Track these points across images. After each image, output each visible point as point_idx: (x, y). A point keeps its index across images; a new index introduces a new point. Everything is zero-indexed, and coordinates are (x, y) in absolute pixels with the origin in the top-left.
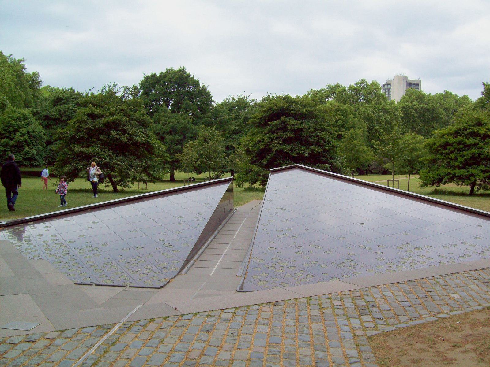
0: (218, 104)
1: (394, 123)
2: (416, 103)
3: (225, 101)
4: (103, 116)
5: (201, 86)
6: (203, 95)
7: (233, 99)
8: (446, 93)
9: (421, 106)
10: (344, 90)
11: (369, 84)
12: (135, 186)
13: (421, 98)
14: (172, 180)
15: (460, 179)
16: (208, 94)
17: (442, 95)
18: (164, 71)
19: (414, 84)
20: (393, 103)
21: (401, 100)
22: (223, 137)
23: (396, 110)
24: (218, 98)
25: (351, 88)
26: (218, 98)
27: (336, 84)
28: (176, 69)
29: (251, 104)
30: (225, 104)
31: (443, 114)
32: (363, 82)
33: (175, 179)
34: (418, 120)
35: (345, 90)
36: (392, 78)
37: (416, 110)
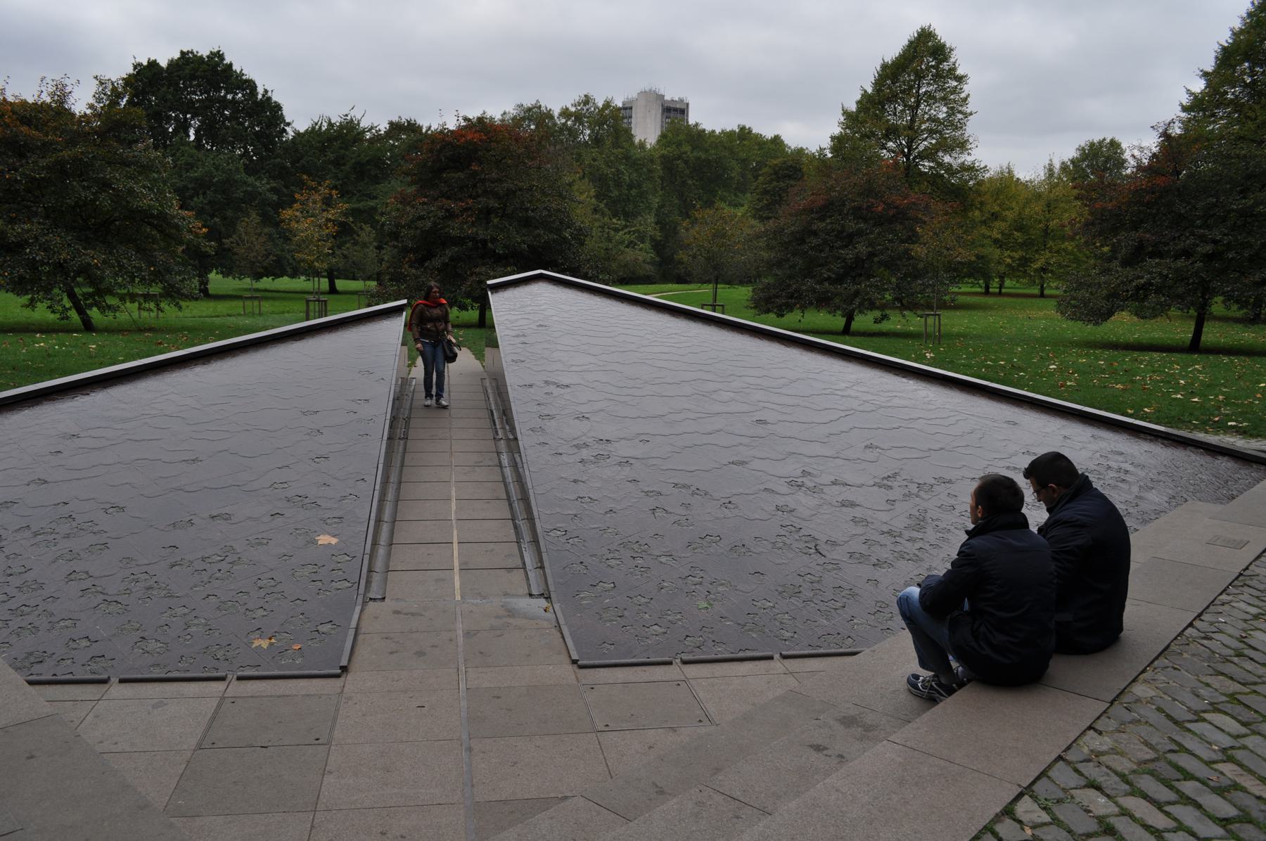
0: (298, 134)
1: (647, 186)
2: (686, 148)
3: (313, 128)
4: (46, 148)
5: (260, 90)
6: (269, 112)
7: (330, 124)
8: (743, 129)
9: (695, 154)
10: (549, 115)
11: (600, 105)
12: (130, 312)
13: (698, 137)
14: (206, 294)
15: (823, 302)
16: (278, 107)
17: (733, 132)
18: (177, 55)
19: (676, 110)
20: (642, 145)
21: (659, 141)
22: (915, 234)
23: (652, 161)
24: (299, 117)
25: (565, 113)
26: (299, 117)
27: (534, 102)
28: (204, 52)
29: (368, 136)
30: (313, 132)
31: (735, 171)
32: (587, 100)
33: (211, 292)
34: (690, 182)
35: (551, 117)
36: (635, 96)
37: (686, 162)
